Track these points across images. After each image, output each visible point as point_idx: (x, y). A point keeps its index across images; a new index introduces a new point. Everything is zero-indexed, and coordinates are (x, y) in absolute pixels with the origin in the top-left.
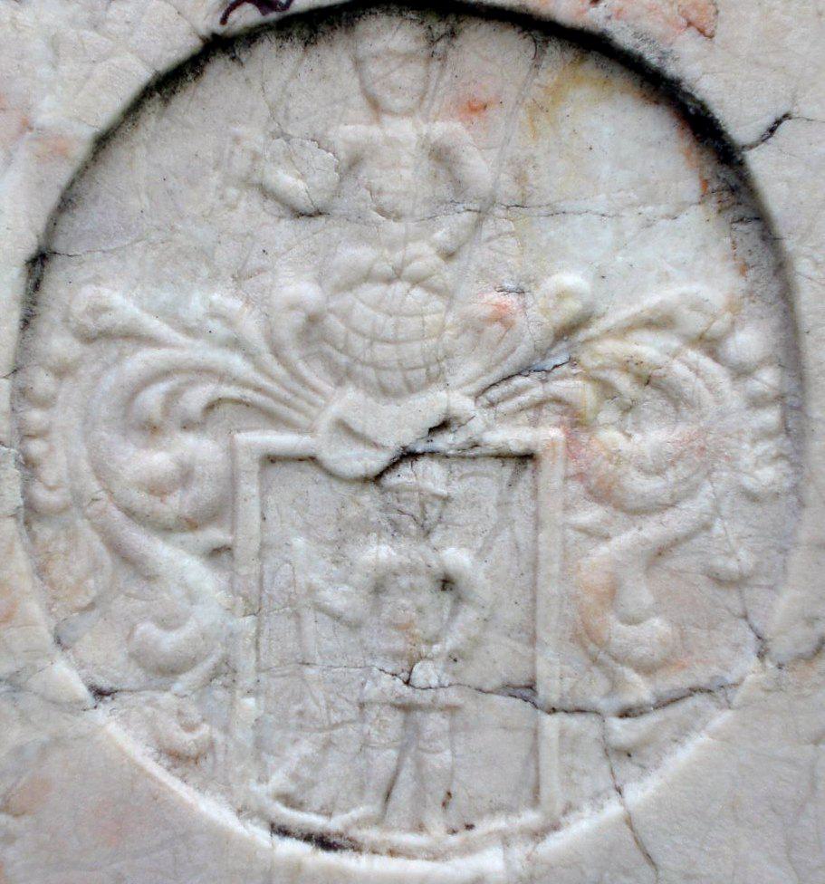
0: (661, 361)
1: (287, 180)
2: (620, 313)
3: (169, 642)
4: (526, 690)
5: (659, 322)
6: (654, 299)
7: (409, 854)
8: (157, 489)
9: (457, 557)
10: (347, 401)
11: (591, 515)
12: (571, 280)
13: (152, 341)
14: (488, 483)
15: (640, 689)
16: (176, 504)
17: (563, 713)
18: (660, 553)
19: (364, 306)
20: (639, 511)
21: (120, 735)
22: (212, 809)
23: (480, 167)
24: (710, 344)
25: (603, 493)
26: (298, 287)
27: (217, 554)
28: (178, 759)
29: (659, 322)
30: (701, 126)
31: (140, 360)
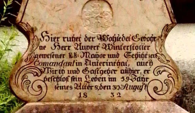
0: (106, 5)
1: (92, 5)
2: (106, 11)
3: (87, 24)
4: (102, 27)
5: (107, 12)
6: (107, 11)
7: (25, 86)
8: (87, 18)
9: (99, 21)
10: (94, 15)
11: (105, 19)
12: (104, 10)
13: (86, 12)
14: (100, 18)
15: (106, 27)
16: (87, 19)
17: (16, 62)
18: (107, 21)
19: (95, 11)
20: (106, 19)
21: (86, 28)
22: (89, 31)
23: (100, 5)
24: (109, 13)
25: (105, 18)
26: (93, 10)
27: (90, 21)
28: (88, 29)
29: (107, 12)
30: (109, 4)
31: (86, 13)
